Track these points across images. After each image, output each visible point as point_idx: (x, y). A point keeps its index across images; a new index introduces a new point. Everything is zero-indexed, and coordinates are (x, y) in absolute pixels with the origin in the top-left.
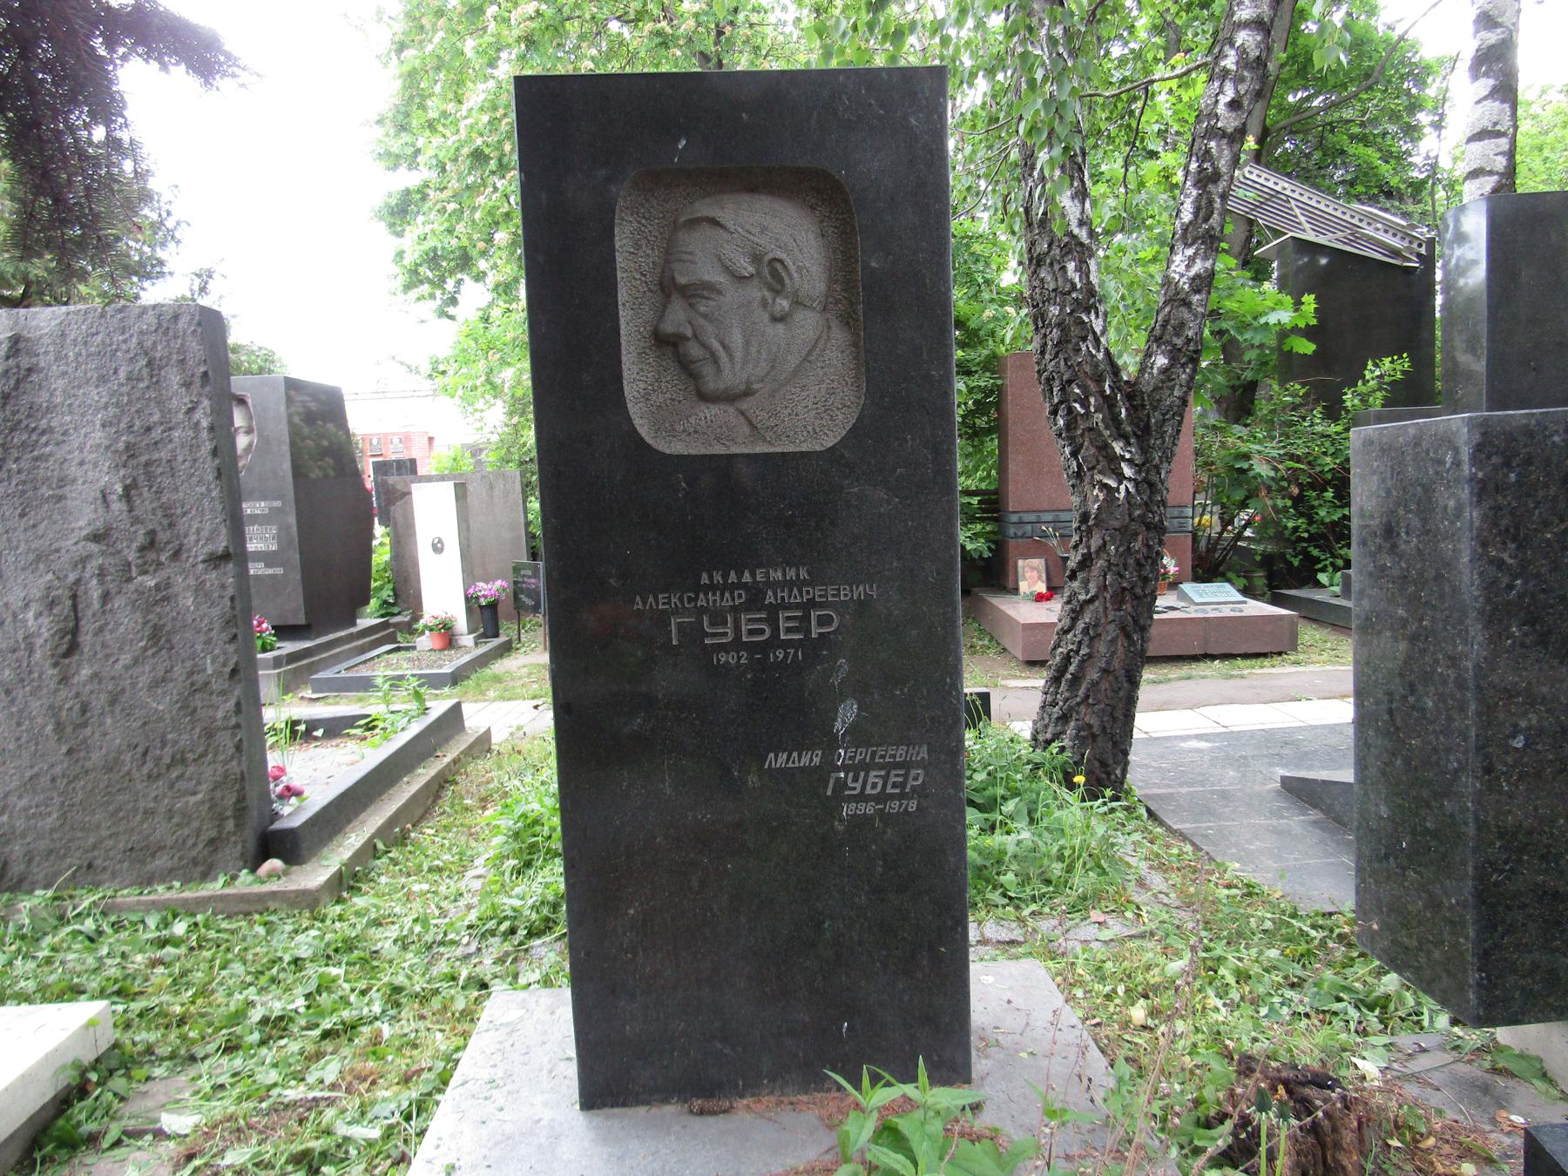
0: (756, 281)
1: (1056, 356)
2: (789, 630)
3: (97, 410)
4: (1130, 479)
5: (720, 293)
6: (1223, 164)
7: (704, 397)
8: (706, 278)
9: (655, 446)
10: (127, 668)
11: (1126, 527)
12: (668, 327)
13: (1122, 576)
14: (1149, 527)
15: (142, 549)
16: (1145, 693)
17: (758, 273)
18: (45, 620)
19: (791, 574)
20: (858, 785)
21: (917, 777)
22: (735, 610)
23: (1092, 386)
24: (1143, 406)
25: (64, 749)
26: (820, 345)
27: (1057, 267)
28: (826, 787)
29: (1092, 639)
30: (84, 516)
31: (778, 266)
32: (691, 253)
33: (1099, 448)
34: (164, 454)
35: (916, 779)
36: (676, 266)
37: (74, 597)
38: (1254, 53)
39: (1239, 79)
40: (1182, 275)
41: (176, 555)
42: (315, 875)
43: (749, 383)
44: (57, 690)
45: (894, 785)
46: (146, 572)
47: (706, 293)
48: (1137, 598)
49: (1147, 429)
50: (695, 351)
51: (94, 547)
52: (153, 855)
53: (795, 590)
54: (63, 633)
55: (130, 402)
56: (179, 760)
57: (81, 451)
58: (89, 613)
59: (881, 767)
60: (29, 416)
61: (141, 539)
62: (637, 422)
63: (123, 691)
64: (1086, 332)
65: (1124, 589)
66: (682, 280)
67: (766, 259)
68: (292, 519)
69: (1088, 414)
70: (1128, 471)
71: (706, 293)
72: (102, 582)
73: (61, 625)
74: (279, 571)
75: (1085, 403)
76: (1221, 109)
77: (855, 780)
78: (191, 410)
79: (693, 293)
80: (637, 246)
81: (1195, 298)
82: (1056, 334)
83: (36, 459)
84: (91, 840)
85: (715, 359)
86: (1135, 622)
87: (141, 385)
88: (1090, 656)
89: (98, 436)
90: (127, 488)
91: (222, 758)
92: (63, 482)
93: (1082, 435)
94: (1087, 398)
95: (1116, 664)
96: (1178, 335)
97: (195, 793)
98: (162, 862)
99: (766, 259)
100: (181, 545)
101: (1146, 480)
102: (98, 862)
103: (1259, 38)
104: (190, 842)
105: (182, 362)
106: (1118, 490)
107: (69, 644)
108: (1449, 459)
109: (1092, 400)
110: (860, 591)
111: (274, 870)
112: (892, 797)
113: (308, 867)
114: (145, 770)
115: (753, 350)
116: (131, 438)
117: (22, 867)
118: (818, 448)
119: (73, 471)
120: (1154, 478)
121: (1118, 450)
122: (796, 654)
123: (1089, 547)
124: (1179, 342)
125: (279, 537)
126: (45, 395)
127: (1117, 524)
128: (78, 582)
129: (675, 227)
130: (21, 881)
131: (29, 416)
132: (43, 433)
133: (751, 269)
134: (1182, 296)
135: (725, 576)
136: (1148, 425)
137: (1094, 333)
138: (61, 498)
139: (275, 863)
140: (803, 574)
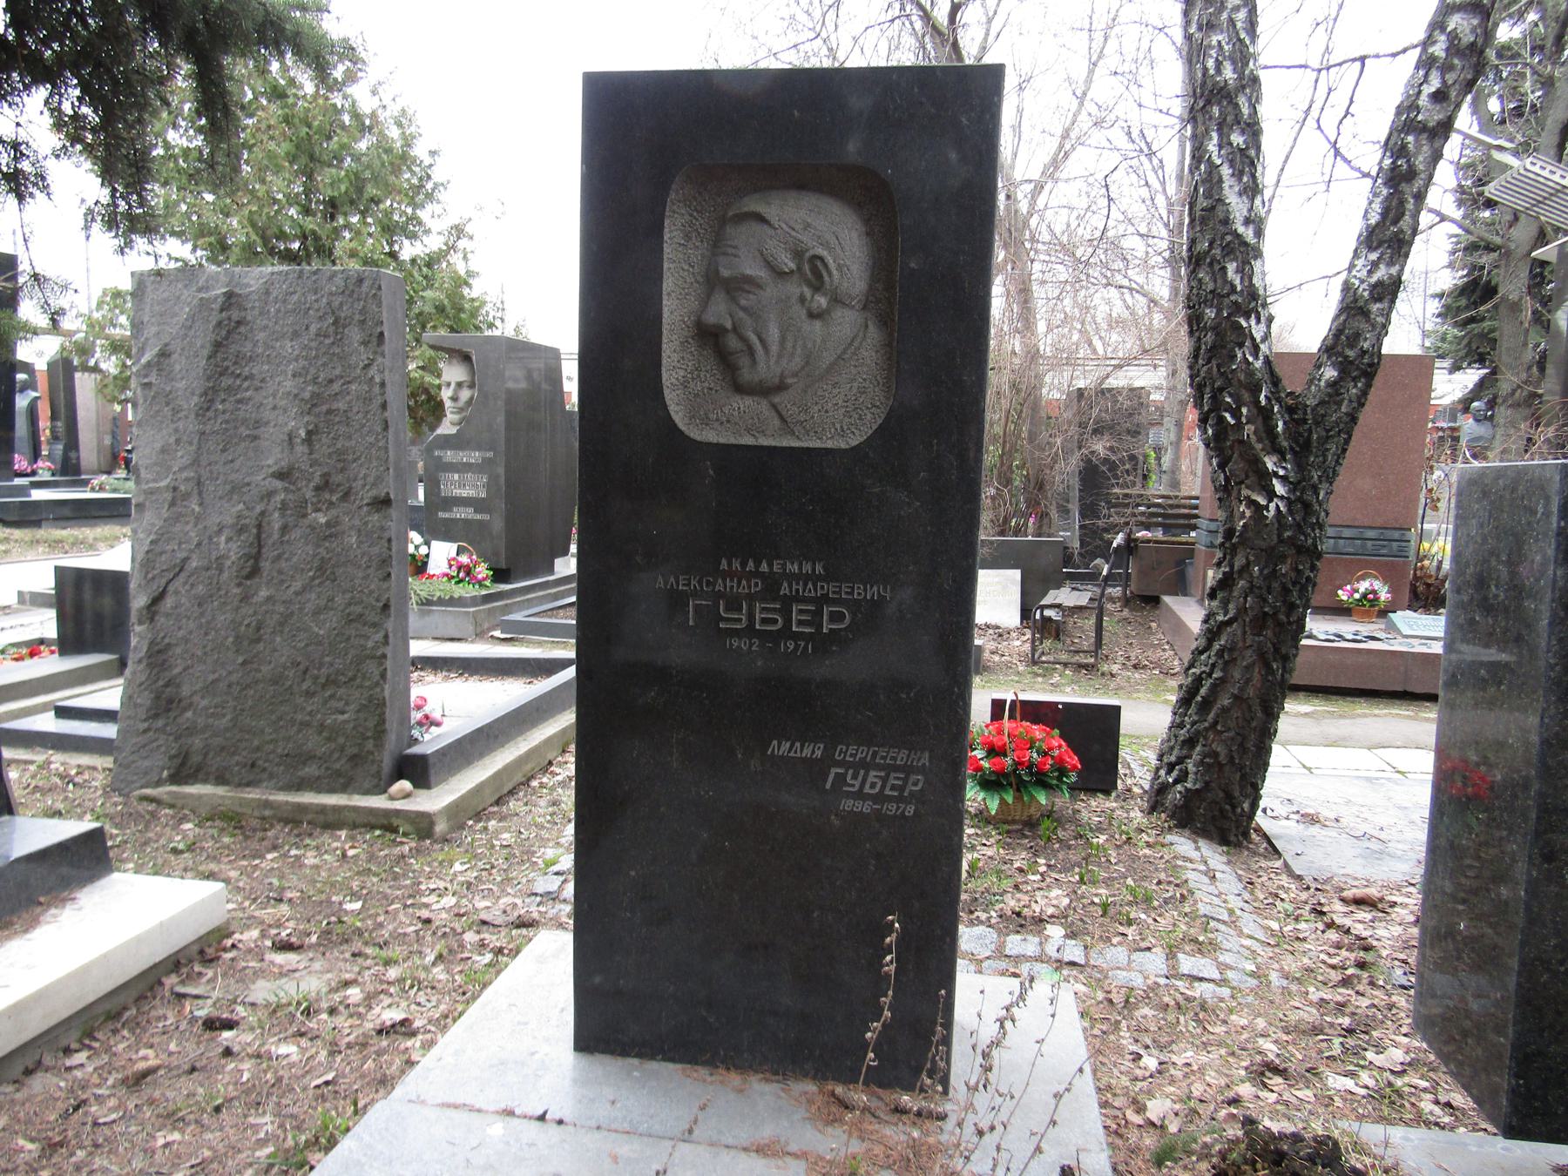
0: (796, 277)
1: (1209, 362)
2: (800, 623)
3: (289, 362)
4: (1282, 497)
5: (759, 286)
6: (1420, 162)
7: (740, 389)
8: (748, 272)
9: (687, 432)
10: (297, 593)
11: (1273, 548)
12: (710, 319)
13: (1265, 600)
14: (1301, 550)
15: (317, 489)
16: (1284, 725)
17: (799, 269)
18: (234, 546)
19: (807, 568)
20: (857, 784)
21: (916, 784)
22: (751, 598)
23: (1246, 396)
24: (1305, 421)
25: (240, 660)
26: (856, 344)
27: (1217, 267)
28: (825, 781)
29: (1226, 663)
30: (274, 458)
31: (819, 264)
32: (735, 247)
33: (1248, 461)
34: (341, 405)
35: (915, 784)
36: (721, 259)
37: (259, 526)
38: (1468, 38)
39: (1446, 68)
40: (1362, 281)
41: (346, 496)
42: (434, 801)
43: (782, 376)
44: (238, 608)
45: (893, 788)
46: (319, 510)
47: (746, 287)
48: (1279, 624)
49: (1306, 446)
50: (733, 343)
51: (278, 484)
52: (304, 764)
53: (810, 585)
54: (248, 557)
55: (316, 357)
56: (330, 682)
57: (274, 396)
58: (270, 542)
59: (879, 767)
60: (235, 363)
61: (317, 480)
62: (672, 408)
63: (292, 613)
64: (1243, 336)
65: (1266, 614)
66: (725, 273)
67: (807, 255)
68: (501, 470)
69: (1239, 426)
70: (1279, 489)
71: (746, 287)
72: (283, 516)
73: (247, 550)
74: (486, 517)
75: (1236, 414)
76: (1423, 101)
77: (855, 777)
78: (367, 367)
79: (737, 286)
80: (687, 237)
81: (1375, 307)
82: (1209, 338)
83: (239, 401)
84: (256, 743)
85: (751, 352)
86: (1277, 650)
87: (327, 341)
88: (1222, 680)
89: (289, 385)
90: (309, 433)
91: (367, 684)
92: (258, 424)
93: (1232, 447)
94: (1239, 408)
95: (1251, 692)
96: (1351, 347)
97: (343, 713)
98: (311, 770)
99: (807, 255)
100: (351, 488)
101: (1299, 499)
102: (260, 762)
103: (1475, 22)
104: (336, 755)
105: (363, 322)
106: (1267, 508)
107: (252, 569)
108: (1540, 509)
109: (1244, 410)
110: (873, 592)
111: (402, 790)
112: (890, 799)
113: (434, 791)
114: (304, 687)
115: (789, 345)
116: (316, 389)
117: (200, 758)
118: (843, 446)
119: (267, 414)
120: (1309, 496)
121: (1270, 466)
122: (806, 648)
123: (1232, 566)
124: (1351, 353)
125: (488, 486)
126: (249, 346)
127: (1263, 545)
128: (263, 513)
129: (723, 222)
130: (198, 770)
131: (235, 363)
132: (246, 378)
133: (792, 265)
134: (1361, 303)
135: (744, 564)
136: (1308, 442)
137: (1253, 339)
138: (256, 438)
139: (405, 785)
140: (819, 569)
